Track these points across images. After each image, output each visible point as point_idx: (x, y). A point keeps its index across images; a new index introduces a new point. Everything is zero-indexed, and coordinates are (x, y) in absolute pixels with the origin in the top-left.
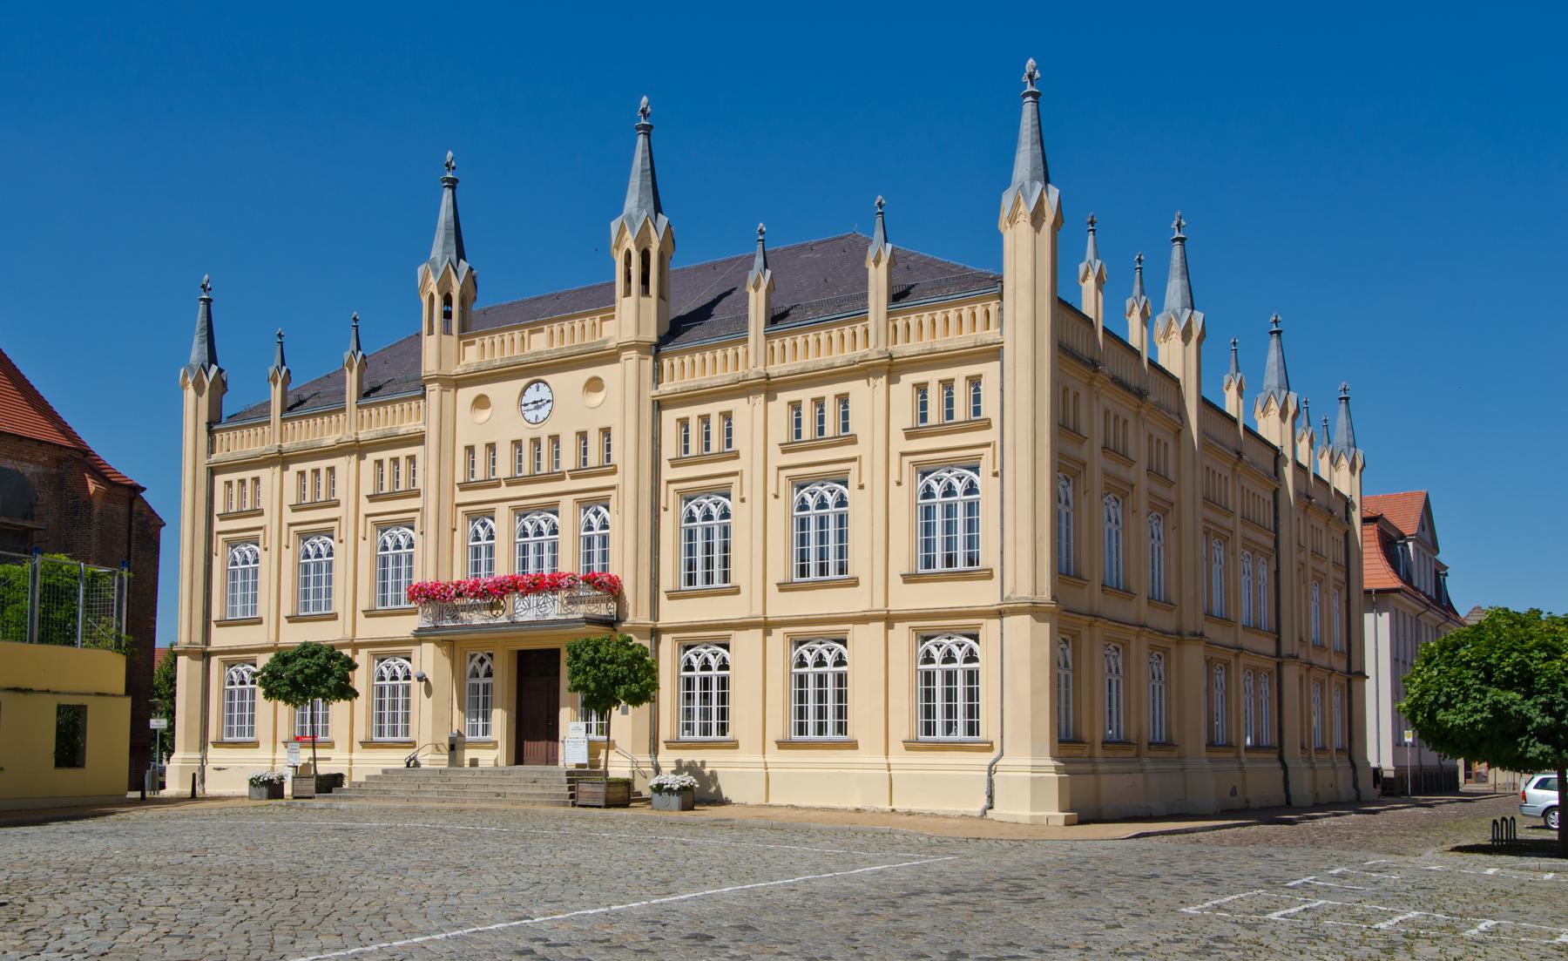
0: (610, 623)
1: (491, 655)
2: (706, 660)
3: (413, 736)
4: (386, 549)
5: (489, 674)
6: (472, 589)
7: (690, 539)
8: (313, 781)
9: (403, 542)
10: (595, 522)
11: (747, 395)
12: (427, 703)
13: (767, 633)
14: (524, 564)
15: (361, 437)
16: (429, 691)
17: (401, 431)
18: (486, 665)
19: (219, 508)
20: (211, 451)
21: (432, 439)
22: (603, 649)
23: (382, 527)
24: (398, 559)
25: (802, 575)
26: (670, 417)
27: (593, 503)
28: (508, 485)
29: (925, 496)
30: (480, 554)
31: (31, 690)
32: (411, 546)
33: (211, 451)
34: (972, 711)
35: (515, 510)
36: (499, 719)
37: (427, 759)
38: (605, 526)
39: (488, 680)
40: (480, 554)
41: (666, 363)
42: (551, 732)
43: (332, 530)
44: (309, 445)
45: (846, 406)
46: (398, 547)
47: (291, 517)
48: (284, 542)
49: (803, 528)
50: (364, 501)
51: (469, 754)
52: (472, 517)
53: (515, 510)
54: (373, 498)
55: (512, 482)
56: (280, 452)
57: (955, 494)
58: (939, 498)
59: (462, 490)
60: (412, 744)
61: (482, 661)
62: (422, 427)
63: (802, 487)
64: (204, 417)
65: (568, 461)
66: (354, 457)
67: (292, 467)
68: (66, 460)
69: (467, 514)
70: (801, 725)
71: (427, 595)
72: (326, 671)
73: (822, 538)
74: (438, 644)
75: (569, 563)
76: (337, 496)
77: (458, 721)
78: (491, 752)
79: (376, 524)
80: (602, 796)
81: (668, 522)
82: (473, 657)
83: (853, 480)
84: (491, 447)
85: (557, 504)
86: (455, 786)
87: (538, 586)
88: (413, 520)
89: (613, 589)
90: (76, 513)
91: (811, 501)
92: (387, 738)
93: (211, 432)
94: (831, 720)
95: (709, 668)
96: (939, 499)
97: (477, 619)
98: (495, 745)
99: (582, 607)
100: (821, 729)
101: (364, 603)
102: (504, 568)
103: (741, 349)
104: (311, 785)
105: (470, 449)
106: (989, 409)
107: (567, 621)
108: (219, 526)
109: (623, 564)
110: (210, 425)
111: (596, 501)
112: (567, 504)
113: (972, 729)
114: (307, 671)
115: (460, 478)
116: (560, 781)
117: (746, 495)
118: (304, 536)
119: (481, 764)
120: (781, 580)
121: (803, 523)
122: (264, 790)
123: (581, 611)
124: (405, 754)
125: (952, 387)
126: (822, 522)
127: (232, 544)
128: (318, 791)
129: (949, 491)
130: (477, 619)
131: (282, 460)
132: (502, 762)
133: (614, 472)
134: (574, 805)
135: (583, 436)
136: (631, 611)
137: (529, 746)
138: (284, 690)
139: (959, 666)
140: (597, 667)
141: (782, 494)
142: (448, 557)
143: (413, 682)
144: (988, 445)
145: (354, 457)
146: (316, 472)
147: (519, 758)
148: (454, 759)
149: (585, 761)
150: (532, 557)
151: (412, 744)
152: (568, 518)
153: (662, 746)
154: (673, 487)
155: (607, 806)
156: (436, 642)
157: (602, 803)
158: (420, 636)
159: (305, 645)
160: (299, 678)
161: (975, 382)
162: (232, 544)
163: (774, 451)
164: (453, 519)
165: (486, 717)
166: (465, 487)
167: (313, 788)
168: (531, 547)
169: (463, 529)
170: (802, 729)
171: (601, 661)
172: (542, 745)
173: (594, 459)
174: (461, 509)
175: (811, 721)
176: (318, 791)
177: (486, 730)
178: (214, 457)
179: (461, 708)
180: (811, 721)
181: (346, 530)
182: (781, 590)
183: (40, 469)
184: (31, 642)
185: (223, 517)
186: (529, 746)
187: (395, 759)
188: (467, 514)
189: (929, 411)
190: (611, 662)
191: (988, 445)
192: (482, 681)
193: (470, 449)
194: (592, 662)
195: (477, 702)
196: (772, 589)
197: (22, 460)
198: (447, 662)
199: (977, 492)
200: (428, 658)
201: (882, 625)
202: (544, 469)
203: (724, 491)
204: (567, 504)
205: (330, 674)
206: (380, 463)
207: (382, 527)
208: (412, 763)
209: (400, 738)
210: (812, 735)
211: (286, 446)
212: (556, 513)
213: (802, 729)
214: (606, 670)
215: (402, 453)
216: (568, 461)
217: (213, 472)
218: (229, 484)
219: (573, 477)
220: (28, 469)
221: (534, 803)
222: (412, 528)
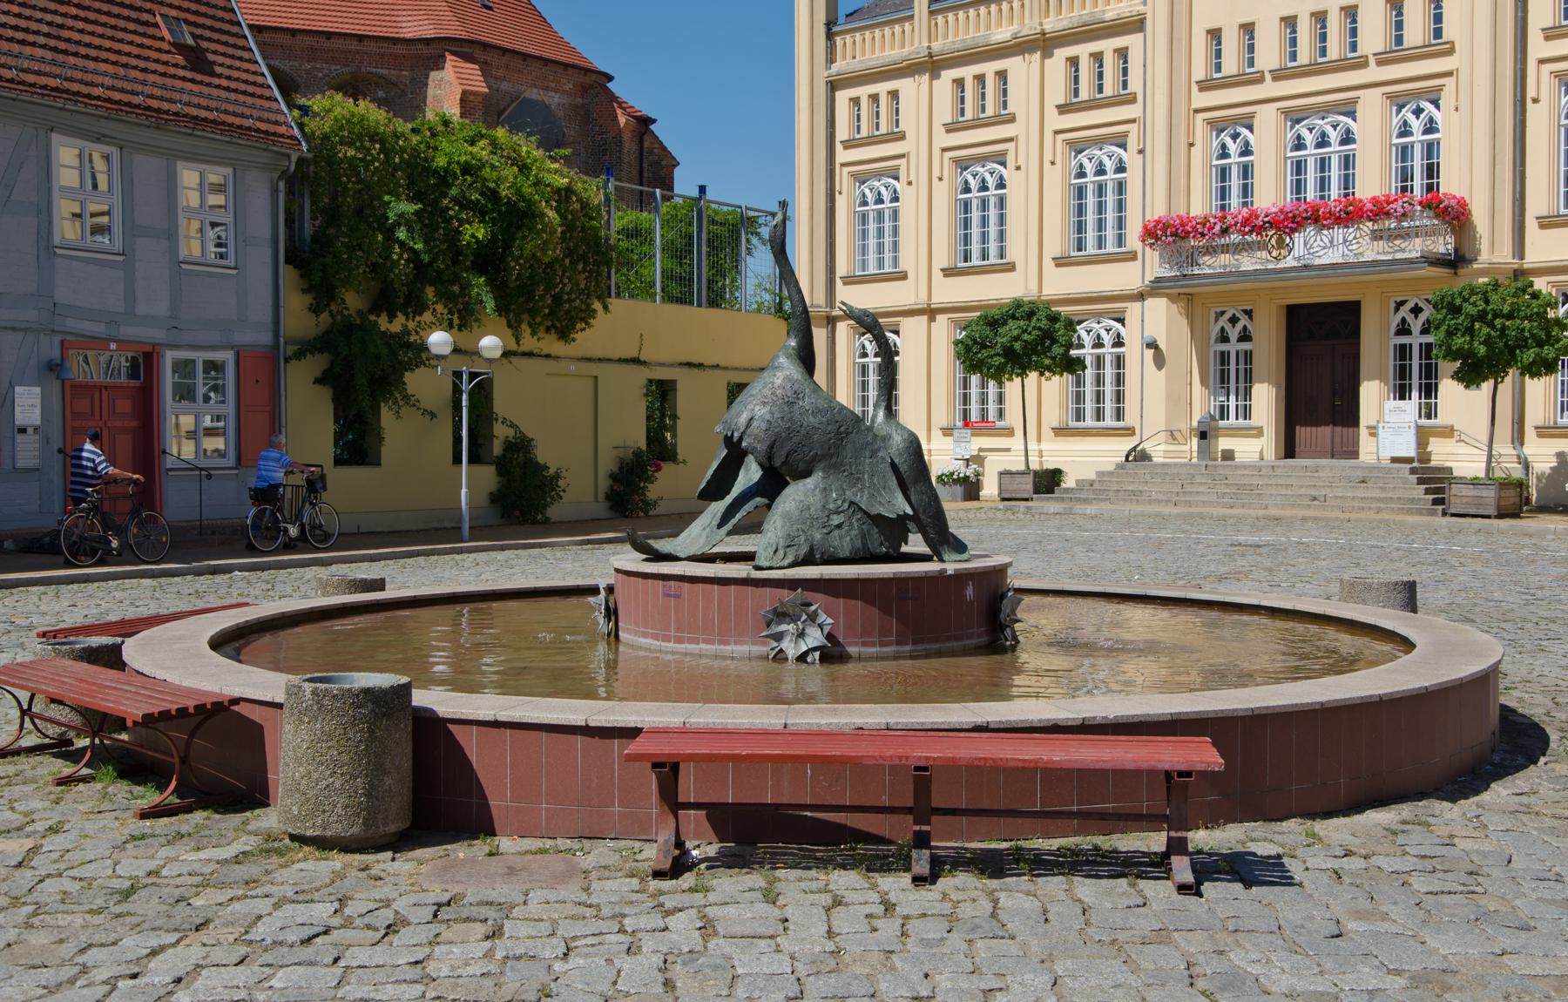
0: (1456, 261)
1: (1249, 313)
2: (1099, 336)
3: (1131, 419)
4: (865, 203)
5: (1245, 337)
6: (1246, 222)
7: (1223, 180)
8: (1030, 479)
9: (886, 195)
10: (1233, 147)
11: (1022, 52)
12: (1157, 380)
13: (932, 319)
14: (1299, 187)
15: (1048, 27)
16: (1159, 361)
17: (1109, 16)
18: (1239, 326)
19: (842, 133)
20: (831, 59)
21: (1158, 24)
22: (1494, 297)
23: (1077, 148)
24: (880, 216)
25: (1080, 249)
26: (843, 97)
27: (1415, 98)
28: (1275, 79)
29: (1402, 134)
30: (1232, 175)
31: (700, 366)
32: (1121, 169)
33: (831, 59)
34: (1119, 396)
35: (1286, 113)
36: (1265, 399)
37: (1159, 450)
38: (1246, 151)
39: (1246, 346)
40: (1232, 175)
41: (838, 40)
42: (1347, 414)
43: (1004, 153)
44: (970, 43)
45: (1354, 21)
46: (880, 201)
47: (1055, 121)
48: (936, 173)
49: (1223, 180)
50: (939, 130)
51: (1224, 443)
52: (1217, 127)
53: (1286, 113)
54: (1063, 109)
55: (1279, 75)
56: (930, 55)
57: (1411, 134)
58: (1091, 177)
59: (1201, 90)
60: (1130, 431)
61: (1234, 320)
62: (1141, 9)
63: (1298, 121)
64: (821, 18)
65: (1269, 55)
66: (926, 77)
67: (1057, 52)
68: (591, 87)
69: (1210, 122)
70: (1078, 410)
71: (1168, 233)
72: (1048, 336)
73: (1101, 208)
74: (1173, 299)
75: (1372, 183)
76: (902, 127)
77: (1201, 402)
78: (1254, 441)
79: (1069, 143)
80: (1492, 502)
81: (841, 203)
82: (1399, 305)
83: (1446, 99)
84: (1248, 29)
85: (1252, 116)
86: (1240, 487)
87: (1317, 217)
88: (1125, 135)
89: (1455, 217)
90: (604, 152)
91: (1309, 139)
92: (1089, 422)
93: (830, 36)
94: (1109, 406)
95: (1409, 332)
96: (1091, 178)
97: (1248, 263)
98: (1258, 432)
99: (1418, 241)
100: (1099, 415)
101: (1054, 247)
102: (1270, 195)
103: (907, 26)
104: (1027, 485)
105: (1215, 35)
106: (1135, 85)
107: (1394, 262)
108: (842, 155)
109: (1466, 175)
110: (830, 24)
111: (1236, 121)
112: (1372, 105)
113: (1119, 414)
114: (1026, 337)
115: (1199, 73)
116: (1405, 481)
117: (912, 178)
118: (963, 165)
119: (1239, 458)
120: (945, 265)
121: (1081, 192)
122: (959, 489)
123: (1414, 248)
124: (1126, 444)
125: (1252, 32)
126: (1323, 164)
127: (861, 179)
128: (1037, 491)
129: (1323, 142)
130: (1248, 263)
131: (932, 65)
132: (1270, 455)
133: (1450, 52)
134: (1444, 514)
135: (1290, 22)
136: (1484, 246)
137: (1302, 433)
138: (998, 361)
139: (1108, 350)
140: (1491, 325)
141: (1058, 161)
142: (1183, 181)
143: (1133, 351)
144: (1133, 121)
145: (1038, 55)
146: (874, 98)
147: (1289, 449)
148: (1205, 452)
149: (1412, 453)
150: (1311, 176)
151: (1130, 431)
152: (1373, 126)
153: (1530, 433)
154: (846, 170)
155: (1500, 516)
156: (1168, 296)
157: (1492, 511)
158: (1157, 288)
159: (1018, 304)
160: (1017, 346)
161: (1122, 53)
162: (861, 179)
163: (939, 130)
164: (1190, 130)
165: (1248, 394)
166: (1205, 86)
167: (1030, 487)
168: (992, 201)
169: (1205, 143)
170: (1079, 415)
171: (1496, 316)
172: (1325, 432)
173: (1415, 33)
174: (1200, 116)
175: (1089, 406)
176: (1037, 491)
177: (1246, 412)
178: (835, 68)
179: (1204, 382)
180: (1089, 406)
181: (915, 168)
182: (1057, 265)
183: (566, 100)
184: (699, 305)
185: (848, 145)
186: (1302, 433)
187: (1110, 452)
188: (1210, 122)
189: (1328, 44)
190: (1510, 316)
191: (1133, 121)
192: (1233, 347)
193: (1215, 35)
194: (1482, 316)
195: (1229, 374)
196: (1048, 264)
197: (547, 88)
198: (1184, 322)
199: (1353, 141)
200: (1158, 319)
201: (925, 318)
202: (883, 130)
203: (1119, 141)
204: (1372, 105)
205: (1054, 341)
206: (959, 83)
207: (963, 165)
208: (1138, 456)
209: (1109, 421)
210: (1089, 422)
211: (937, 46)
212: (1352, 114)
213: (1079, 415)
214: (1504, 328)
215: (1107, 46)
216: (1269, 55)
217: (833, 86)
218: (856, 101)
219: (1380, 63)
220: (554, 99)
221: (1379, 511)
222: (897, 178)
